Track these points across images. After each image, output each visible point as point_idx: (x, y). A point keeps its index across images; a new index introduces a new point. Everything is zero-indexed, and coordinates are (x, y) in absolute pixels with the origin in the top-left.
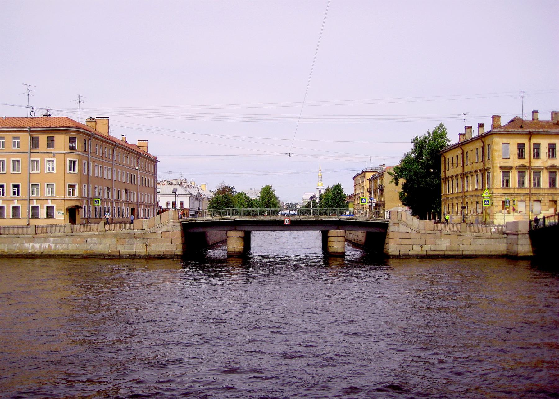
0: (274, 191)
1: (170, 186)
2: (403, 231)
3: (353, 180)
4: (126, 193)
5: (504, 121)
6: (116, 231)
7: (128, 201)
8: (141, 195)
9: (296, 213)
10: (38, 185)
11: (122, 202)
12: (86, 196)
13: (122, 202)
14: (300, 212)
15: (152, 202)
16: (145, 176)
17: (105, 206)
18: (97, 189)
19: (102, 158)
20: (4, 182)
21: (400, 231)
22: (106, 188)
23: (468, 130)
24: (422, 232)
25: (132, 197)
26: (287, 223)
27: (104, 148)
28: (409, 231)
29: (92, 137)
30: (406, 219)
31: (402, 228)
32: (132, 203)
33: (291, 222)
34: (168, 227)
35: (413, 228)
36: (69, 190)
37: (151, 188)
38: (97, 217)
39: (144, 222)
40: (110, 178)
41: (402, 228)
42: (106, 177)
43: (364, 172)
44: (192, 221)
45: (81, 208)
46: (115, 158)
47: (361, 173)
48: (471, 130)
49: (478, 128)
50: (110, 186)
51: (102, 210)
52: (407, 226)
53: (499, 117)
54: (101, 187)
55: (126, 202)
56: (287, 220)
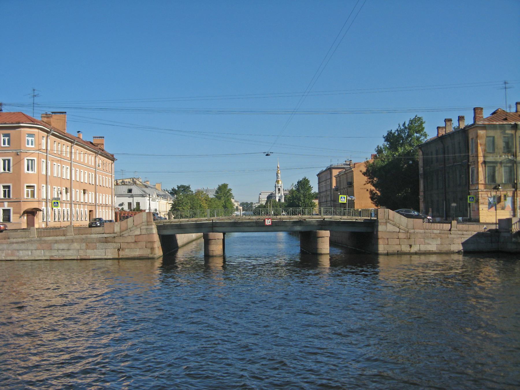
0: (230, 190)
1: (124, 186)
2: (391, 231)
3: (317, 178)
4: (84, 193)
5: (486, 114)
6: (85, 235)
7: (78, 202)
8: (99, 195)
9: (252, 213)
10: (33, 186)
11: (80, 204)
12: (45, 197)
13: (80, 204)
14: (333, 212)
15: (93, 202)
16: (102, 175)
17: (63, 209)
18: (56, 190)
19: (60, 156)
20: (10, 183)
21: (388, 230)
22: (65, 188)
23: (448, 123)
24: (412, 231)
25: (90, 198)
26: (268, 224)
27: (62, 145)
28: (398, 230)
29: (51, 133)
30: (394, 218)
31: (390, 227)
32: (90, 205)
33: (272, 222)
34: (141, 230)
35: (401, 227)
36: (27, 191)
37: (105, 187)
38: (56, 220)
39: (115, 225)
40: (69, 178)
41: (390, 227)
42: (64, 177)
43: (330, 169)
44: (167, 224)
45: (41, 210)
46: (73, 157)
47: (326, 170)
48: (451, 123)
49: (459, 120)
50: (69, 187)
51: (60, 213)
52: (394, 225)
53: (482, 109)
54: (59, 188)
55: (85, 204)
56: (268, 221)
